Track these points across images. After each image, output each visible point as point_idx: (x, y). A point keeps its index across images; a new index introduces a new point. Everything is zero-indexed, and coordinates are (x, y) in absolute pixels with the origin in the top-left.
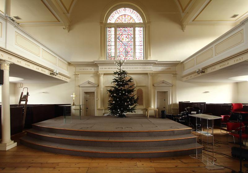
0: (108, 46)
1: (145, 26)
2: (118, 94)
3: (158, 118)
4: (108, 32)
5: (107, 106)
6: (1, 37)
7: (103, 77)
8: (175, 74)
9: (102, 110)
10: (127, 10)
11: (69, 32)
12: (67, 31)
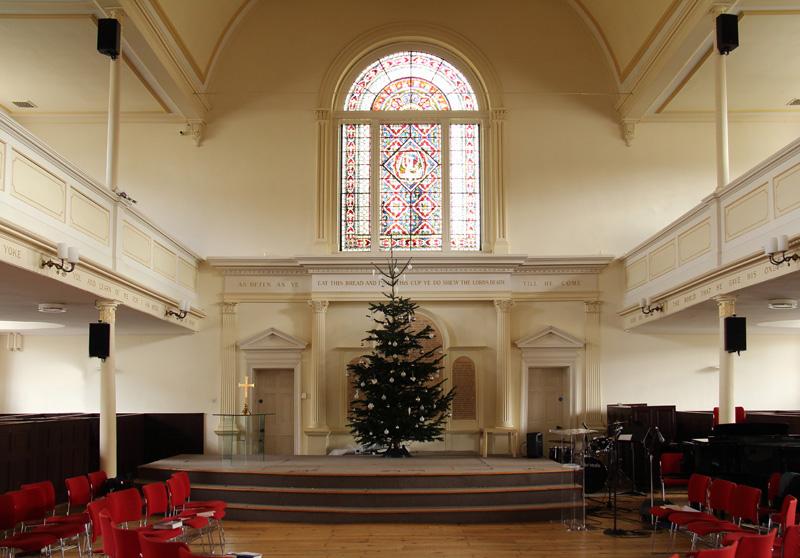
0: (346, 194)
1: (489, 121)
2: (383, 379)
3: (516, 458)
4: (344, 140)
5: (342, 420)
6: (4, 190)
7: (326, 314)
8: (596, 303)
9: (323, 435)
10: (419, 61)
11: (199, 146)
12: (195, 143)
